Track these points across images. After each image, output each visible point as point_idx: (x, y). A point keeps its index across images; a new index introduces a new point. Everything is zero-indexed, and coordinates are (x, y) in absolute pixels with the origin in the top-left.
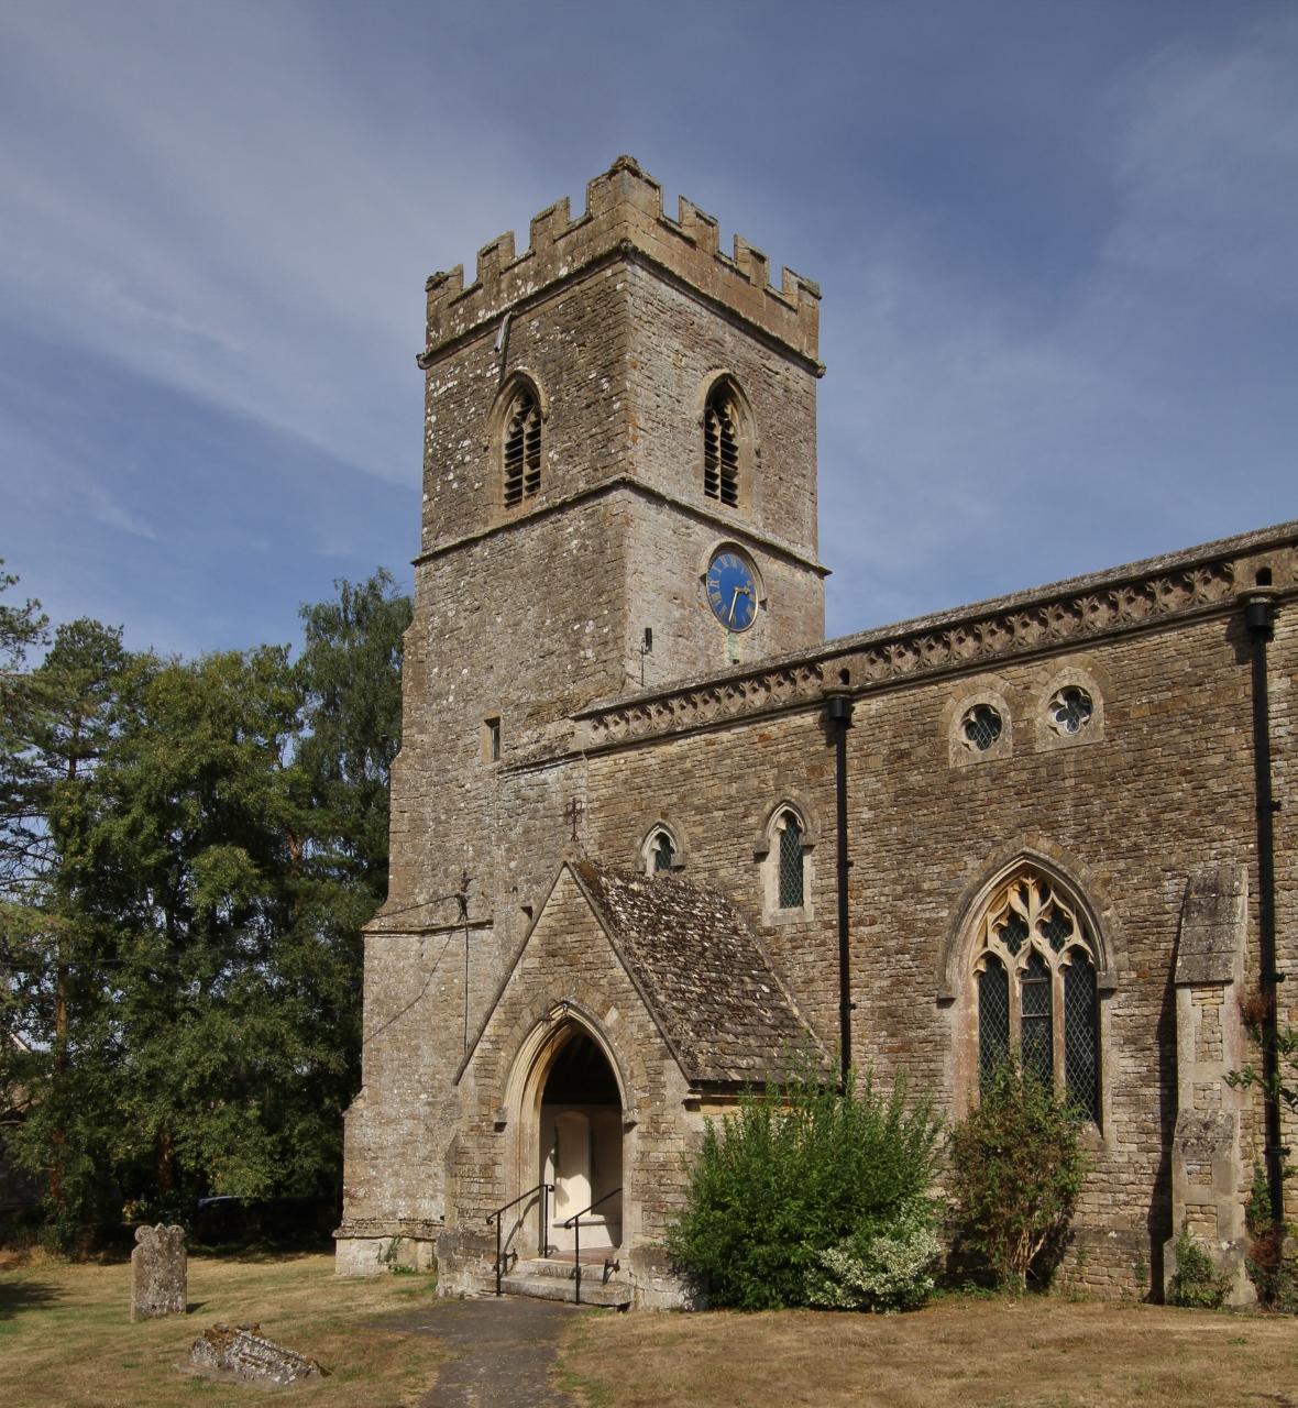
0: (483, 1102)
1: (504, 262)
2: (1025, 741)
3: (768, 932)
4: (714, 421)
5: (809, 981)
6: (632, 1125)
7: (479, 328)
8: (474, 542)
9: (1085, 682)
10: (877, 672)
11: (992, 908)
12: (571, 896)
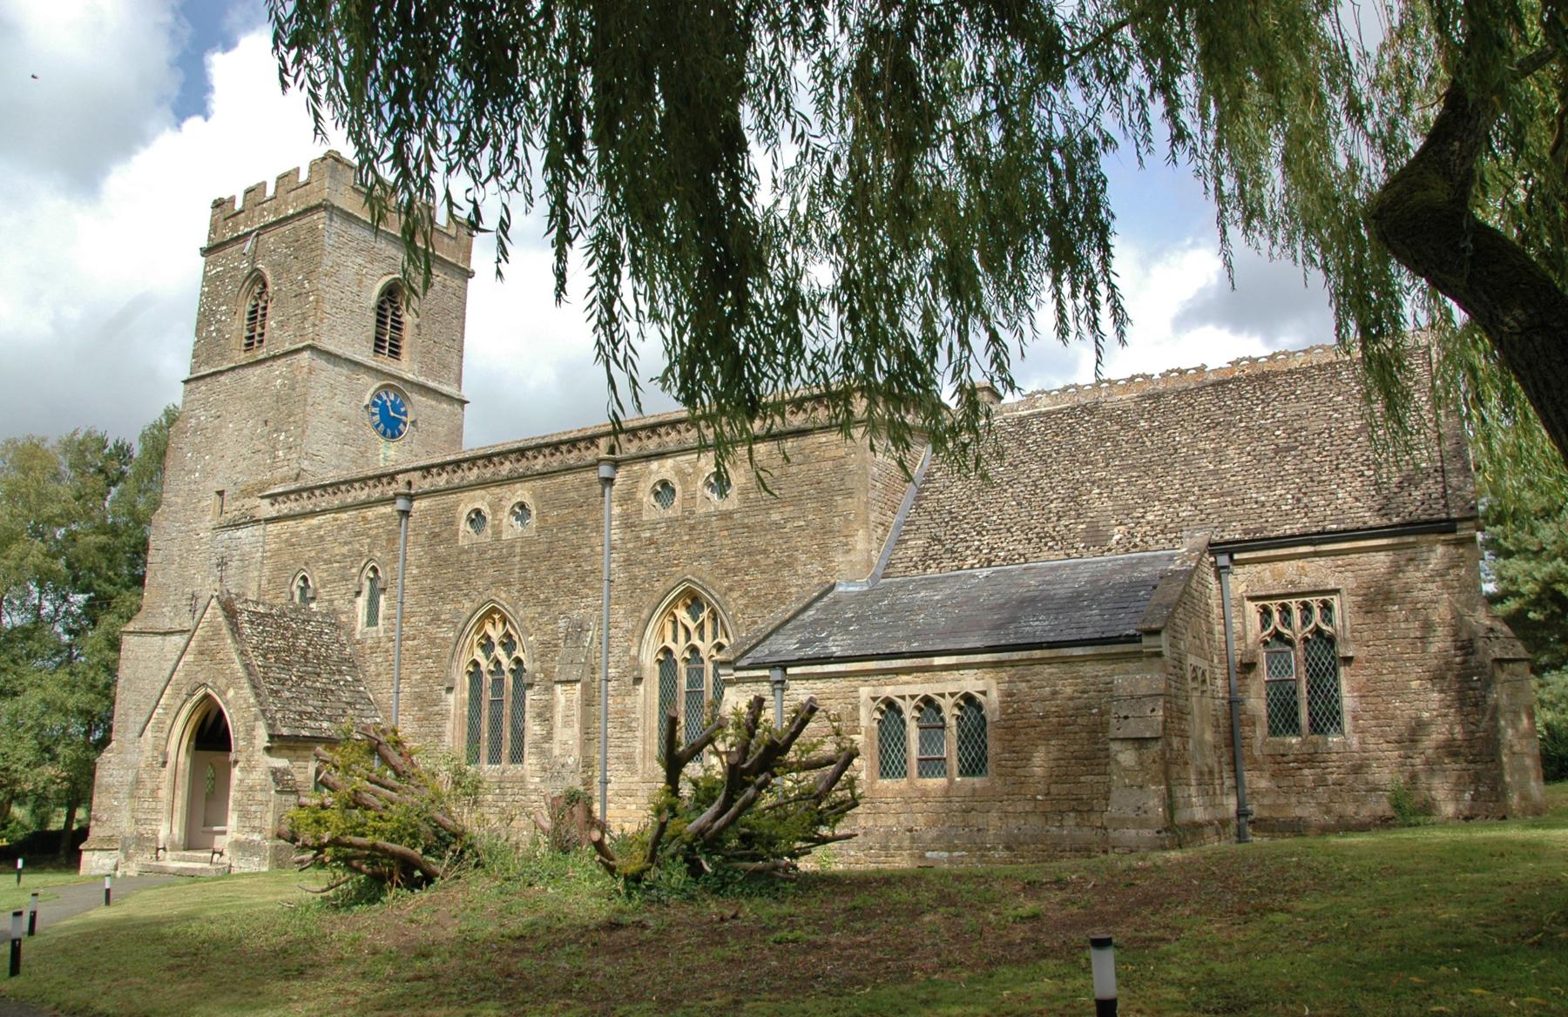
0: (155, 748)
1: (258, 200)
2: (497, 533)
3: (358, 642)
4: (387, 306)
5: (378, 675)
6: (236, 762)
7: (239, 237)
8: (221, 373)
9: (529, 501)
10: (426, 485)
11: (477, 632)
12: (215, 616)
